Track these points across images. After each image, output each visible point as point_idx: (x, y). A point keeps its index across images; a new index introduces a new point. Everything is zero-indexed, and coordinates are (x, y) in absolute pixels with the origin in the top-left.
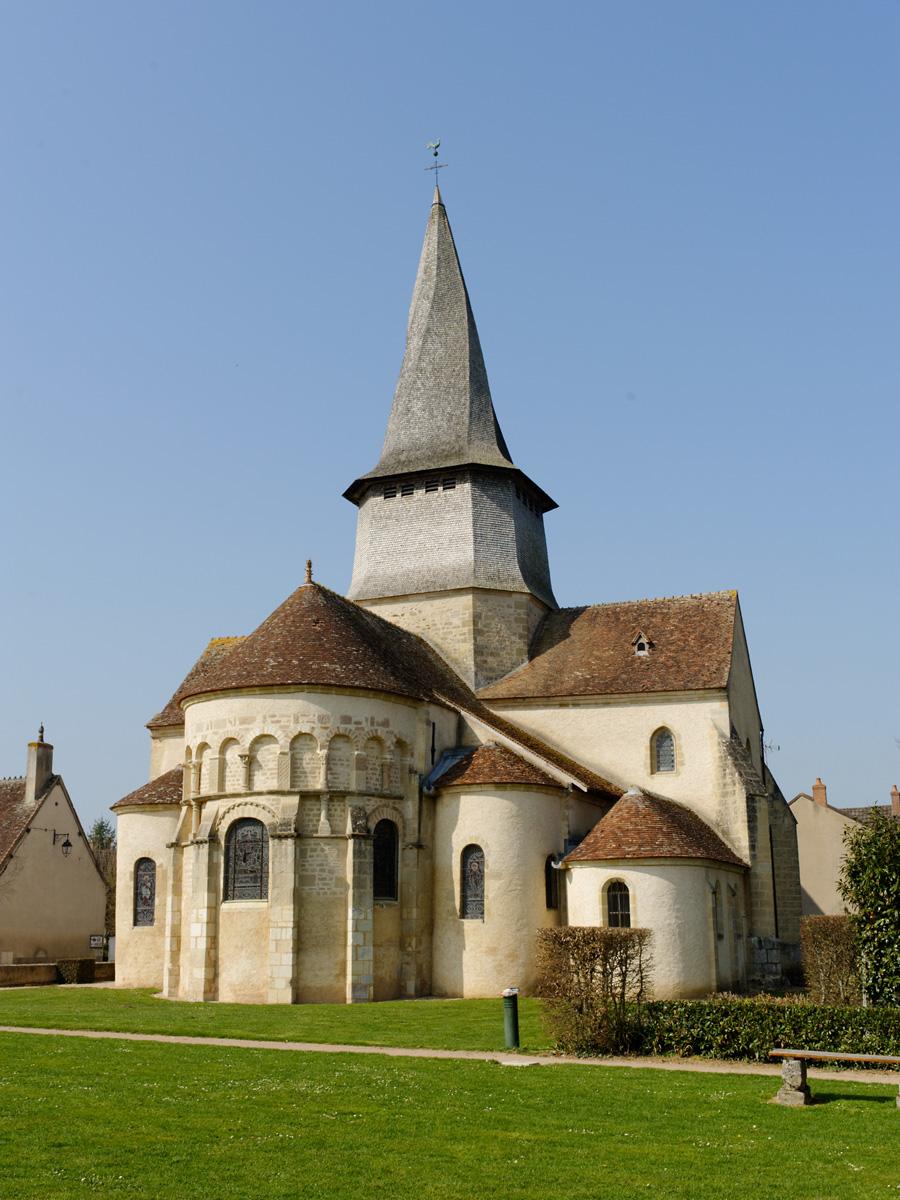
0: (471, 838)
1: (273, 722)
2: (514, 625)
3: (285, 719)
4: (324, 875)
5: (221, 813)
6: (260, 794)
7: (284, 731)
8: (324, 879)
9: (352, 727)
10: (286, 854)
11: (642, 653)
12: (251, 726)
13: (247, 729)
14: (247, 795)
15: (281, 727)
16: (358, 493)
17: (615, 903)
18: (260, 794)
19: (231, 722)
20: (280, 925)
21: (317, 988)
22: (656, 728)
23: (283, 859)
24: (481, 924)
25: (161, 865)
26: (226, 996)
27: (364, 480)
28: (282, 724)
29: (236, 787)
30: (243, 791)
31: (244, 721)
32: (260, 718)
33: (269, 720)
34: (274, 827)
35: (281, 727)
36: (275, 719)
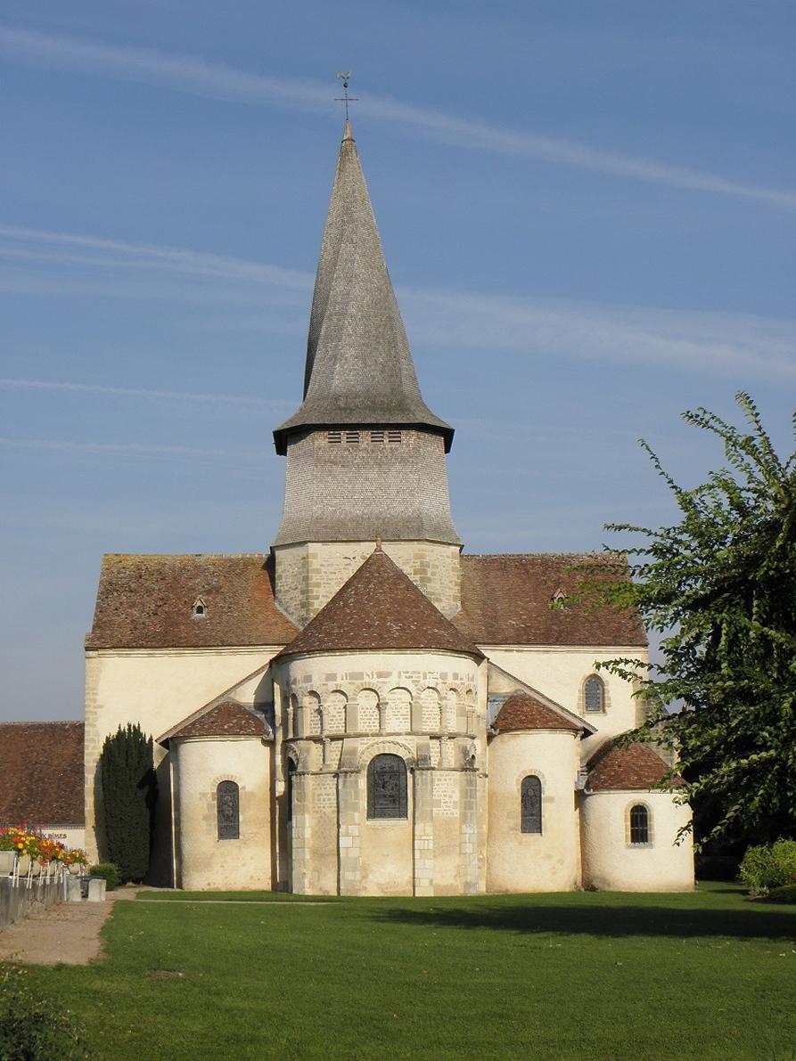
0: (531, 771)
1: (406, 677)
2: (452, 573)
3: (417, 675)
4: (447, 799)
5: (365, 751)
6: (399, 734)
7: (416, 685)
8: (446, 802)
9: (458, 682)
10: (426, 783)
11: (561, 595)
12: (387, 680)
13: (384, 682)
14: (377, 735)
15: (413, 682)
16: (284, 439)
17: (642, 820)
18: (399, 734)
19: (369, 676)
20: (423, 838)
21: (444, 886)
22: (588, 674)
23: (424, 787)
24: (540, 837)
25: (244, 788)
26: (416, 895)
27: (284, 430)
28: (414, 679)
29: (373, 728)
30: (375, 729)
31: (380, 675)
32: (395, 674)
33: (403, 675)
34: (412, 761)
35: (413, 682)
36: (409, 674)
